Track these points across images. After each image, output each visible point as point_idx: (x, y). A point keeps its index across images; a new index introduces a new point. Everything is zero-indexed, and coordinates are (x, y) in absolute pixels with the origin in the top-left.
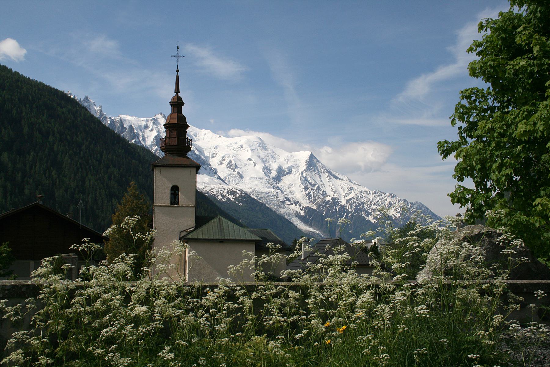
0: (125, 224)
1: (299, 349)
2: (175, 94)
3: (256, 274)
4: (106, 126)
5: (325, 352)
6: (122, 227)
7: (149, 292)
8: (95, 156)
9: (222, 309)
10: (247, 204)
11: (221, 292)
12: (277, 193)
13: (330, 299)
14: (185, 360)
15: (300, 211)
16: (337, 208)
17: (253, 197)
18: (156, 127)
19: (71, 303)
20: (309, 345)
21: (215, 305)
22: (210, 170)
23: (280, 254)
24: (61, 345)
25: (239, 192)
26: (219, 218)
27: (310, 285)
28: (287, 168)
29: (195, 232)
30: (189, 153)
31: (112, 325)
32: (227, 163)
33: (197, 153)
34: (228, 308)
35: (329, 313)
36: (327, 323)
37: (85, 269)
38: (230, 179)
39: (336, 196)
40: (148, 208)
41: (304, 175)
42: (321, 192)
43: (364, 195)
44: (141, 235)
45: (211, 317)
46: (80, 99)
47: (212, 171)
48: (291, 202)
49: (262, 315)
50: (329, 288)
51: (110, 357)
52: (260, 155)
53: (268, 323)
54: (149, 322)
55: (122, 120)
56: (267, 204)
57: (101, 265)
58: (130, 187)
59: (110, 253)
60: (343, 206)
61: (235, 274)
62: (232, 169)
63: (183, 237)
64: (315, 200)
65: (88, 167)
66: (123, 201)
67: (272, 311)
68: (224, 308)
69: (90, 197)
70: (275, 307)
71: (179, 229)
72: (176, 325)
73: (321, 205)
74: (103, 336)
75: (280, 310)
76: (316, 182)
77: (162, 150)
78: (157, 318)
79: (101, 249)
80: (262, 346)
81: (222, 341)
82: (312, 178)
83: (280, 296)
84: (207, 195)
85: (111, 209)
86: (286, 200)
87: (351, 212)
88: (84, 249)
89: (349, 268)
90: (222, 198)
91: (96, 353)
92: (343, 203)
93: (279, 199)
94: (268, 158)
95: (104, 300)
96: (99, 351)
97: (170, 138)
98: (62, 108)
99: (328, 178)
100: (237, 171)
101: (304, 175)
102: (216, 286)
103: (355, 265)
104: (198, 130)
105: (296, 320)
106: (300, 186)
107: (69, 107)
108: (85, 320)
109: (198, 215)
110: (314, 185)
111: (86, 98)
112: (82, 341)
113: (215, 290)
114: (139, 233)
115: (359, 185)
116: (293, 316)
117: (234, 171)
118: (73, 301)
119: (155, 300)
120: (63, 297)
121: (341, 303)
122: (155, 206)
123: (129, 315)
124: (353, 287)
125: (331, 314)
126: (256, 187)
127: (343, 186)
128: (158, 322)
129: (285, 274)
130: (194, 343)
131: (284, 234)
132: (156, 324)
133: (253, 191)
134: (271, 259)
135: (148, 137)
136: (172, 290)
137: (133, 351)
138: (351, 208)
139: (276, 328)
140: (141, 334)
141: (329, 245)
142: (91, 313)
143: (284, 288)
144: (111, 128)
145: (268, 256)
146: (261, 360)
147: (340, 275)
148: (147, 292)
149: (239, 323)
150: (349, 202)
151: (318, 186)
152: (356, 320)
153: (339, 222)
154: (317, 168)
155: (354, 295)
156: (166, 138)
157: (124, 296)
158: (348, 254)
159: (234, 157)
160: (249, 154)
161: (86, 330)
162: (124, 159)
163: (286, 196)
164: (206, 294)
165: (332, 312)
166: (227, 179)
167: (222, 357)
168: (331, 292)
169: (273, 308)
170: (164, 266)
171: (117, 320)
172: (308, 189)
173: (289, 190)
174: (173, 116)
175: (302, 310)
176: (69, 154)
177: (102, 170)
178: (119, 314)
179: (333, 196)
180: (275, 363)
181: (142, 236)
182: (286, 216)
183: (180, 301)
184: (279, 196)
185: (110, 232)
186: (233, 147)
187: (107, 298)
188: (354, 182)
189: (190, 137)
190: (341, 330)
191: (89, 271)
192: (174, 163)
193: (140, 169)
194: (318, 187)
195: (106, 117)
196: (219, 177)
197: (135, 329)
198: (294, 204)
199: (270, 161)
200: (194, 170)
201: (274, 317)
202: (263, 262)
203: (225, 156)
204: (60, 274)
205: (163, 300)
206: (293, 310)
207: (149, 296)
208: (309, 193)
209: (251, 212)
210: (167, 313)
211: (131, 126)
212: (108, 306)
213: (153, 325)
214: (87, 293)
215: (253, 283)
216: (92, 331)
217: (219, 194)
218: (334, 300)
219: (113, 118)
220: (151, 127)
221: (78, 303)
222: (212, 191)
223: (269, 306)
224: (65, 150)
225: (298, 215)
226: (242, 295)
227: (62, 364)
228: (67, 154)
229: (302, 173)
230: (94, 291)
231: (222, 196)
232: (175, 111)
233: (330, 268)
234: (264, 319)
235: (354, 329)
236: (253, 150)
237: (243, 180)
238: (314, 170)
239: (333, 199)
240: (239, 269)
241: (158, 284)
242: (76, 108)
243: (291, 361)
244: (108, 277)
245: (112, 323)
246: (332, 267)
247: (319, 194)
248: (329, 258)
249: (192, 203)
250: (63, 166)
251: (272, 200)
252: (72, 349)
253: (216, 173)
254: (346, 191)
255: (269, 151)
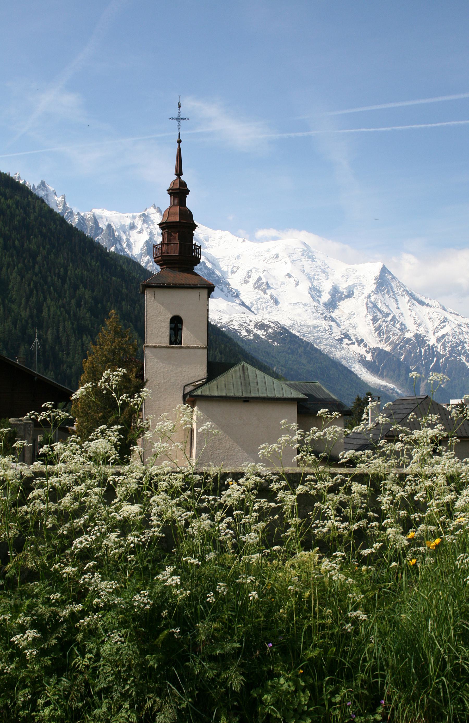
0: (105, 382)
1: (368, 571)
2: (176, 177)
3: (302, 457)
4: (72, 226)
5: (408, 576)
6: (101, 386)
7: (142, 484)
8: (57, 271)
9: (252, 510)
10: (285, 343)
11: (250, 483)
12: (331, 326)
13: (416, 498)
14: (197, 586)
15: (366, 354)
16: (423, 350)
17: (293, 332)
18: (147, 228)
19: (28, 498)
20: (382, 565)
21: (241, 505)
22: (229, 292)
23: (338, 428)
24: (13, 559)
25: (272, 325)
26: (243, 366)
27: (385, 475)
28: (346, 289)
29: (207, 386)
30: (198, 266)
31: (88, 533)
32: (254, 282)
33: (209, 265)
34: (261, 508)
35: (413, 518)
36: (412, 534)
37: (47, 447)
38: (259, 306)
39: (421, 331)
40: (136, 350)
41: (372, 299)
42: (398, 326)
43: (464, 330)
44: (127, 398)
45: (235, 522)
46: (34, 185)
47: (231, 293)
48: (352, 340)
49: (311, 519)
50: (413, 479)
51: (86, 580)
52: (304, 268)
53: (321, 531)
54: (141, 528)
55: (97, 217)
56: (316, 343)
57: (71, 441)
58: (109, 318)
59: (81, 417)
60: (432, 346)
61: (269, 457)
62: (262, 290)
63: (187, 393)
64: (388, 338)
65: (46, 287)
66: (99, 338)
67: (325, 513)
68: (254, 509)
69: (50, 332)
70: (330, 507)
71: (182, 382)
72: (182, 532)
73: (398, 345)
74: (76, 548)
75: (339, 511)
76: (391, 310)
77: (156, 262)
78: (155, 523)
79: (71, 419)
80: (311, 566)
81: (251, 558)
82: (384, 303)
83: (339, 491)
84: (224, 329)
85: (80, 351)
86: (345, 338)
87: (444, 356)
88: (45, 419)
89: (444, 450)
90: (246, 334)
91: (64, 573)
92: (432, 341)
93: (333, 335)
94: (317, 273)
95: (75, 495)
96: (69, 570)
97: (168, 244)
98: (6, 199)
99: (409, 304)
100: (269, 294)
101: (372, 299)
102: (242, 475)
103: (454, 444)
104: (210, 231)
105: (363, 526)
106: (366, 316)
107: (18, 198)
108: (47, 523)
109: (210, 360)
110: (388, 315)
111: (43, 184)
112: (44, 555)
113: (241, 481)
114: (124, 395)
115: (457, 315)
116: (358, 521)
117: (265, 293)
118: (31, 495)
119: (152, 496)
120: (16, 489)
121: (432, 502)
122: (146, 347)
123: (114, 518)
124: (451, 479)
125: (417, 519)
126: (298, 318)
127: (432, 316)
128: (156, 529)
129: (346, 458)
130: (210, 560)
131: (340, 389)
132: (154, 532)
133: (294, 324)
134: (325, 434)
135: (135, 242)
136: (176, 480)
137: (118, 570)
138: (445, 350)
139: (331, 538)
140: (132, 545)
141: (413, 413)
142: (56, 512)
143: (344, 477)
144: (79, 229)
145: (321, 429)
146: (310, 588)
147: (431, 460)
148: (139, 483)
149: (277, 531)
150: (440, 341)
151: (393, 317)
152: (456, 529)
153: (430, 380)
154: (392, 288)
155: (452, 491)
156: (162, 244)
157: (105, 489)
158: (443, 427)
159: (265, 272)
160: (288, 268)
161: (49, 538)
162: (100, 276)
163: (344, 331)
164: (227, 487)
165: (419, 516)
166: (255, 306)
167: (252, 581)
168: (416, 485)
169: (328, 508)
170: (164, 445)
171: (96, 525)
172: (378, 321)
173: (349, 322)
174: (173, 210)
175: (373, 511)
176: (18, 268)
177: (68, 291)
178: (98, 515)
179: (416, 332)
180: (330, 591)
181: (129, 399)
182: (344, 362)
183: (189, 496)
184: (333, 331)
185: (82, 393)
186: (263, 257)
187: (79, 491)
188: (449, 310)
189: (198, 241)
190: (432, 544)
191: (53, 450)
192: (174, 282)
193: (124, 291)
194: (394, 318)
195: (71, 213)
196: (243, 302)
197: (122, 538)
198: (356, 344)
199: (320, 278)
200: (205, 292)
201: (329, 521)
202: (313, 440)
203: (251, 271)
204: (12, 456)
205: (164, 495)
206: (358, 511)
207: (142, 488)
208: (380, 326)
209: (291, 355)
210: (169, 514)
211: (109, 226)
212: (81, 503)
213: (149, 533)
214: (51, 484)
215: (296, 470)
216: (58, 538)
217: (242, 329)
218: (421, 499)
219: (82, 214)
220: (139, 227)
221: (38, 499)
222: (231, 323)
223: (322, 506)
224: (12, 263)
225: (363, 361)
226: (281, 489)
227: (15, 588)
228: (14, 269)
229: (369, 296)
230: (61, 481)
231: (248, 331)
232: (176, 204)
233: (414, 448)
234: (314, 525)
235: (453, 544)
236: (294, 261)
237: (279, 306)
238: (388, 292)
239: (417, 336)
240: (277, 449)
241: (156, 472)
242: (28, 198)
243: (355, 589)
244: (82, 459)
245: (88, 529)
246: (417, 446)
247: (395, 329)
248: (413, 434)
249: (203, 342)
250: (10, 287)
251: (324, 337)
252: (30, 565)
253: (237, 296)
254: (437, 323)
255: (319, 263)
